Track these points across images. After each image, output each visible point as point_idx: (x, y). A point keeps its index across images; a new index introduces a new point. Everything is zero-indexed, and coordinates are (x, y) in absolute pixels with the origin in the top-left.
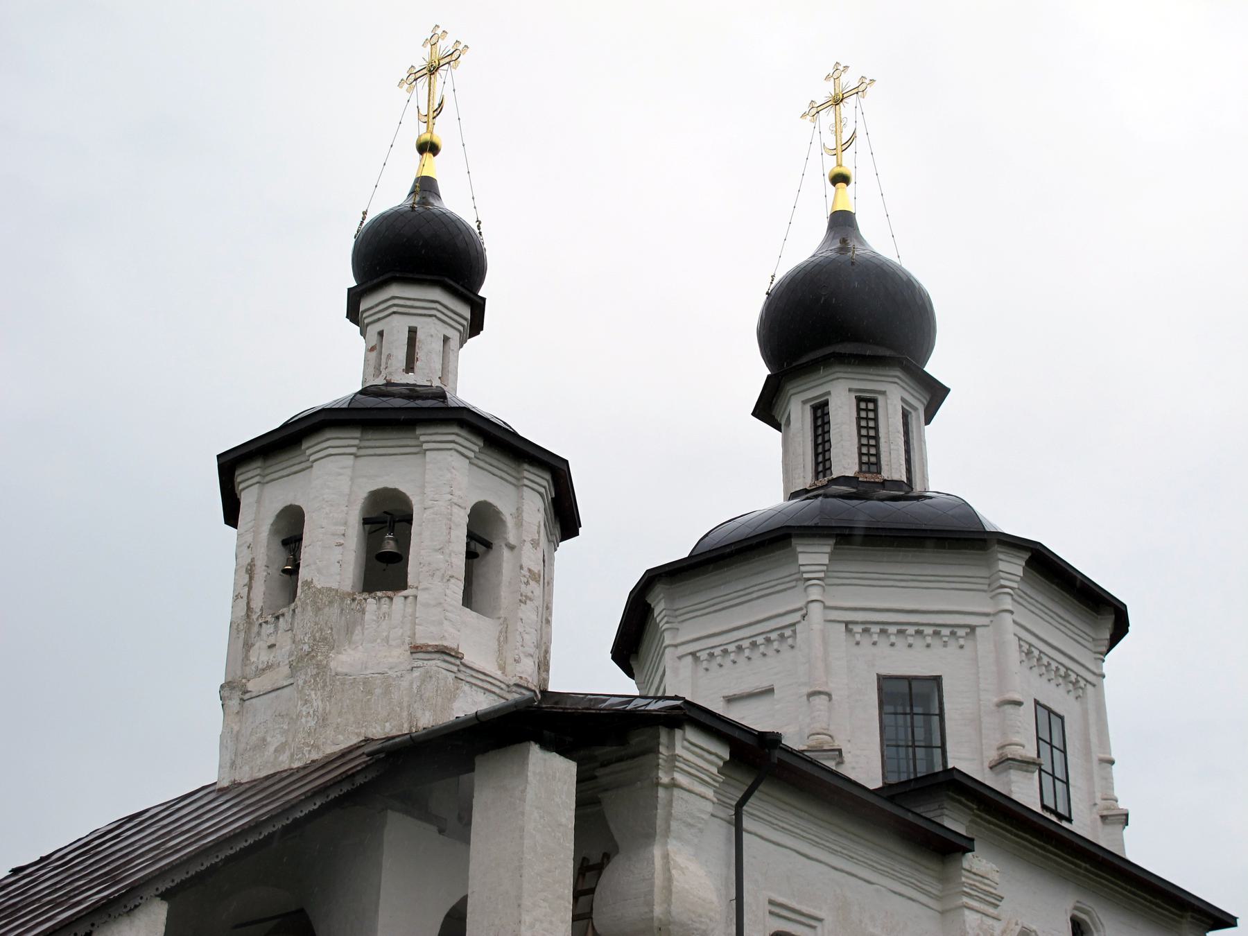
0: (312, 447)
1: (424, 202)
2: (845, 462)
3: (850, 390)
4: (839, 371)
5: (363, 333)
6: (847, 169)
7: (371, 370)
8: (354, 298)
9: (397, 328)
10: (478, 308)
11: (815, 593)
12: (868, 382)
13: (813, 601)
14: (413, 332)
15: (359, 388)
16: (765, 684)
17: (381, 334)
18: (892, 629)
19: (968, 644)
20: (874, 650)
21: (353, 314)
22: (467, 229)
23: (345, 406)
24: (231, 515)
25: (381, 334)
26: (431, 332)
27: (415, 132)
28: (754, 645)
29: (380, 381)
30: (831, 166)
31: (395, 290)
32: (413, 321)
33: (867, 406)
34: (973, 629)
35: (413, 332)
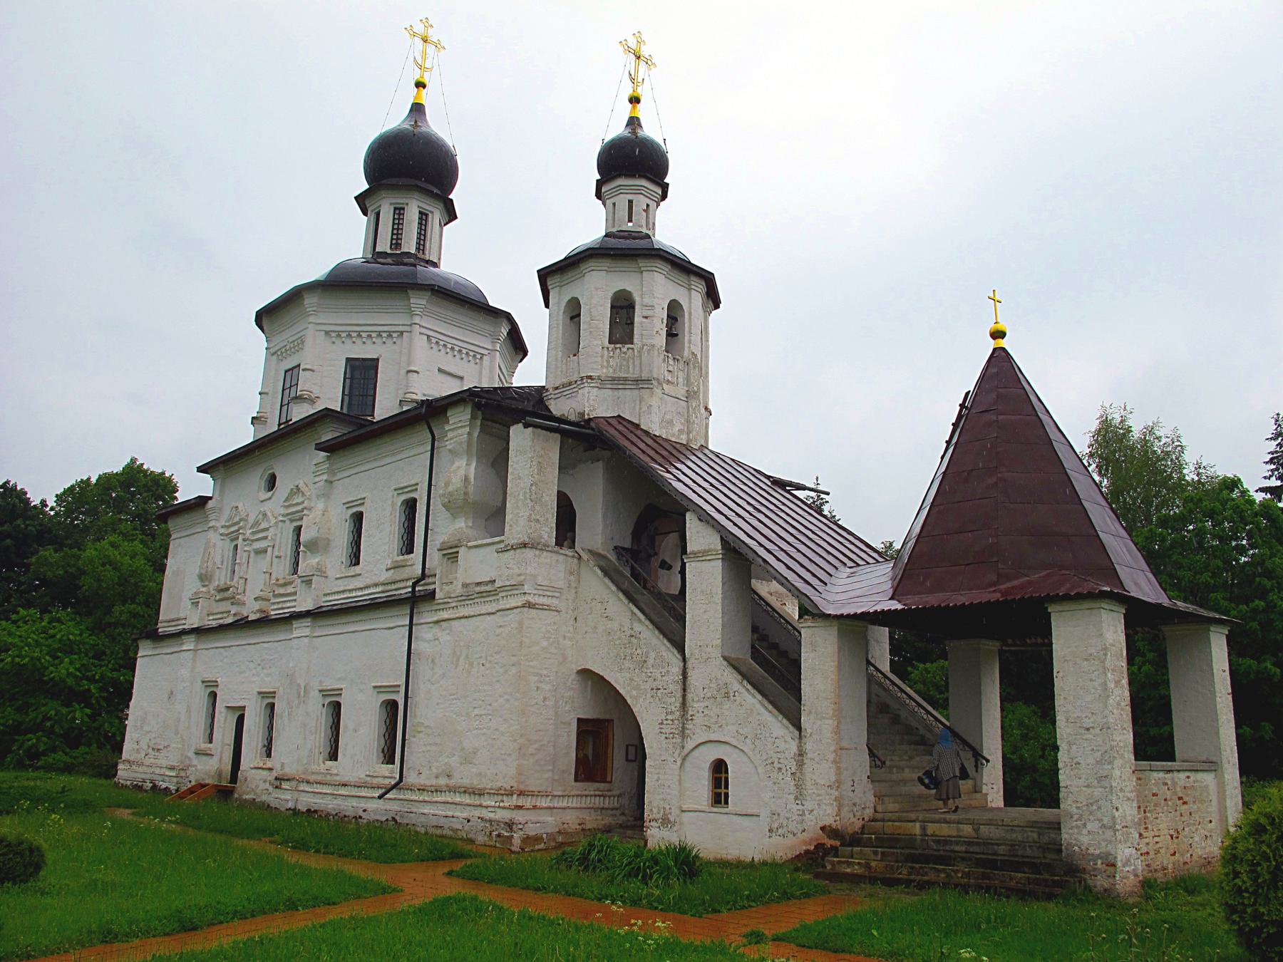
0: (584, 267)
1: (634, 132)
2: (384, 246)
3: (391, 204)
4: (416, 195)
5: (604, 204)
6: (426, 80)
7: (610, 225)
8: (599, 184)
9: (622, 201)
10: (665, 188)
11: (417, 320)
12: (400, 200)
13: (415, 324)
14: (630, 202)
15: (603, 233)
16: (461, 374)
17: (614, 204)
18: (344, 335)
19: (398, 342)
20: (364, 346)
21: (599, 195)
22: (658, 145)
23: (597, 246)
24: (547, 306)
25: (614, 204)
26: (641, 202)
27: (628, 91)
28: (452, 349)
29: (614, 230)
30: (417, 76)
31: (620, 181)
32: (630, 197)
33: (423, 216)
34: (402, 333)
35: (630, 202)
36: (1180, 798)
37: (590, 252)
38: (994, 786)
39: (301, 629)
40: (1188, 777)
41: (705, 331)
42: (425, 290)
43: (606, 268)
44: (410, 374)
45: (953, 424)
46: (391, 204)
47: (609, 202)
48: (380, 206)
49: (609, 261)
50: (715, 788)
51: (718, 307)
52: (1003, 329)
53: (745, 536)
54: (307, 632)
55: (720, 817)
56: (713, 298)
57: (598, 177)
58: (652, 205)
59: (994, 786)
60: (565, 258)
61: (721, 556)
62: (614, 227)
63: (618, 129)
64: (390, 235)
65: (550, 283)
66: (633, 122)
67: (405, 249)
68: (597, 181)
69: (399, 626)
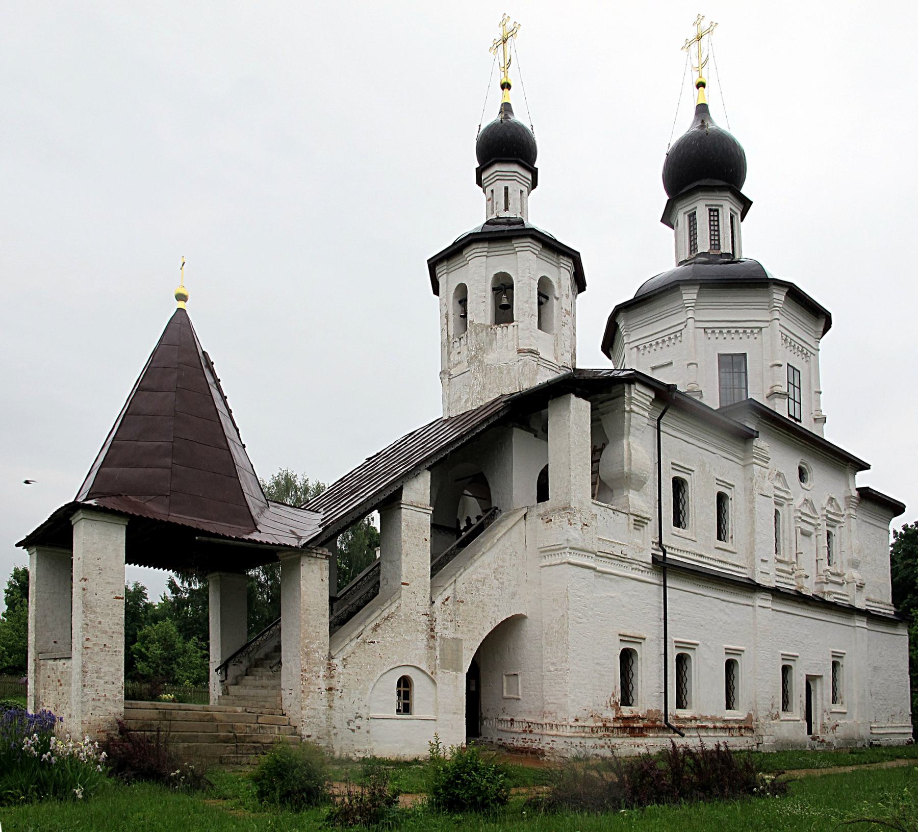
1: (506, 117)
2: (704, 246)
3: (706, 205)
4: (700, 195)
8: (479, 172)
9: (499, 187)
10: (534, 173)
14: (506, 189)
17: (492, 191)
21: (479, 182)
24: (436, 291)
25: (492, 191)
26: (515, 188)
29: (494, 217)
31: (497, 167)
33: (714, 213)
34: (761, 328)
35: (506, 189)
36: (59, 681)
37: (470, 238)
38: (292, 692)
39: (762, 601)
40: (64, 664)
41: (571, 313)
42: (694, 285)
43: (485, 253)
44: (690, 367)
45: (219, 380)
46: (706, 205)
47: (488, 190)
48: (696, 208)
49: (486, 245)
50: (408, 704)
51: (584, 290)
52: (186, 293)
53: (91, 475)
54: (768, 604)
55: (403, 724)
56: (580, 283)
57: (478, 165)
58: (525, 193)
59: (292, 692)
60: (454, 244)
61: (431, 512)
62: (492, 213)
63: (492, 116)
64: (721, 234)
65: (439, 270)
66: (506, 108)
67: (722, 251)
68: (477, 169)
69: (702, 595)
